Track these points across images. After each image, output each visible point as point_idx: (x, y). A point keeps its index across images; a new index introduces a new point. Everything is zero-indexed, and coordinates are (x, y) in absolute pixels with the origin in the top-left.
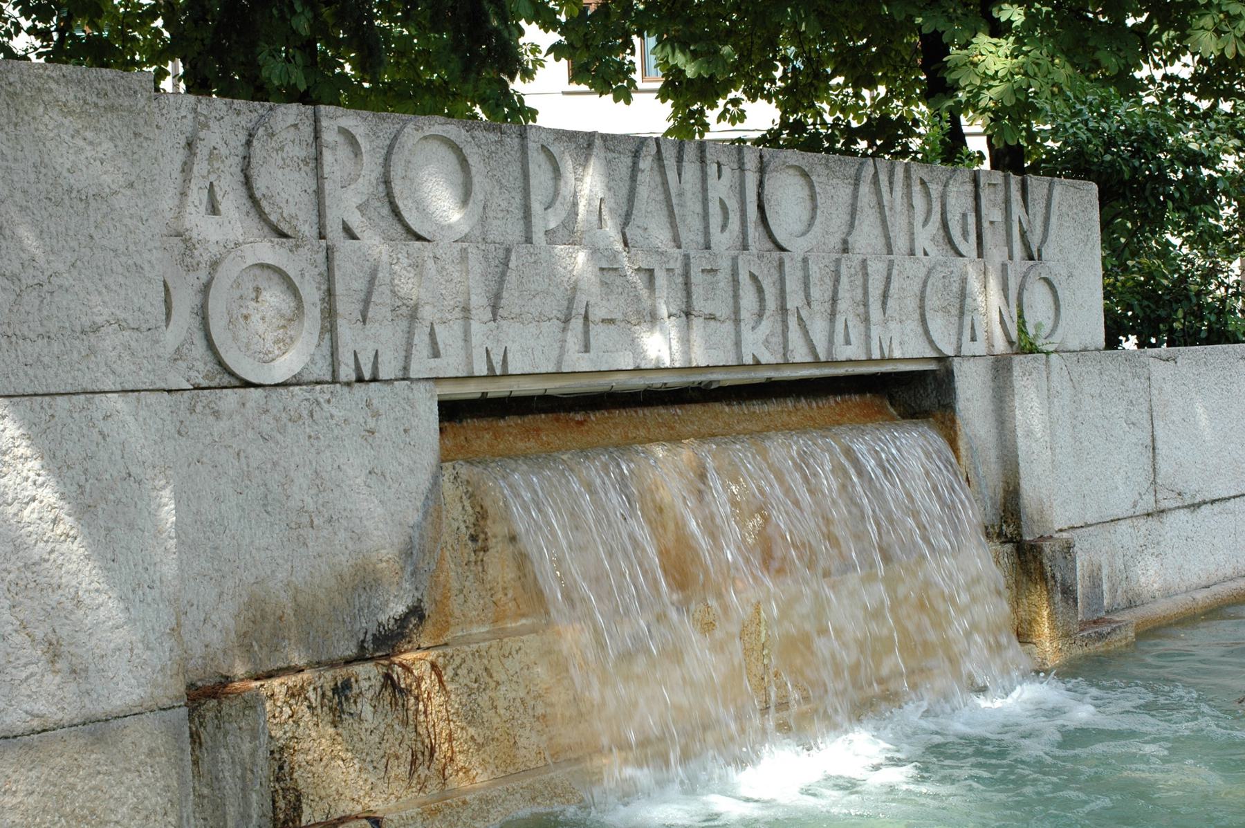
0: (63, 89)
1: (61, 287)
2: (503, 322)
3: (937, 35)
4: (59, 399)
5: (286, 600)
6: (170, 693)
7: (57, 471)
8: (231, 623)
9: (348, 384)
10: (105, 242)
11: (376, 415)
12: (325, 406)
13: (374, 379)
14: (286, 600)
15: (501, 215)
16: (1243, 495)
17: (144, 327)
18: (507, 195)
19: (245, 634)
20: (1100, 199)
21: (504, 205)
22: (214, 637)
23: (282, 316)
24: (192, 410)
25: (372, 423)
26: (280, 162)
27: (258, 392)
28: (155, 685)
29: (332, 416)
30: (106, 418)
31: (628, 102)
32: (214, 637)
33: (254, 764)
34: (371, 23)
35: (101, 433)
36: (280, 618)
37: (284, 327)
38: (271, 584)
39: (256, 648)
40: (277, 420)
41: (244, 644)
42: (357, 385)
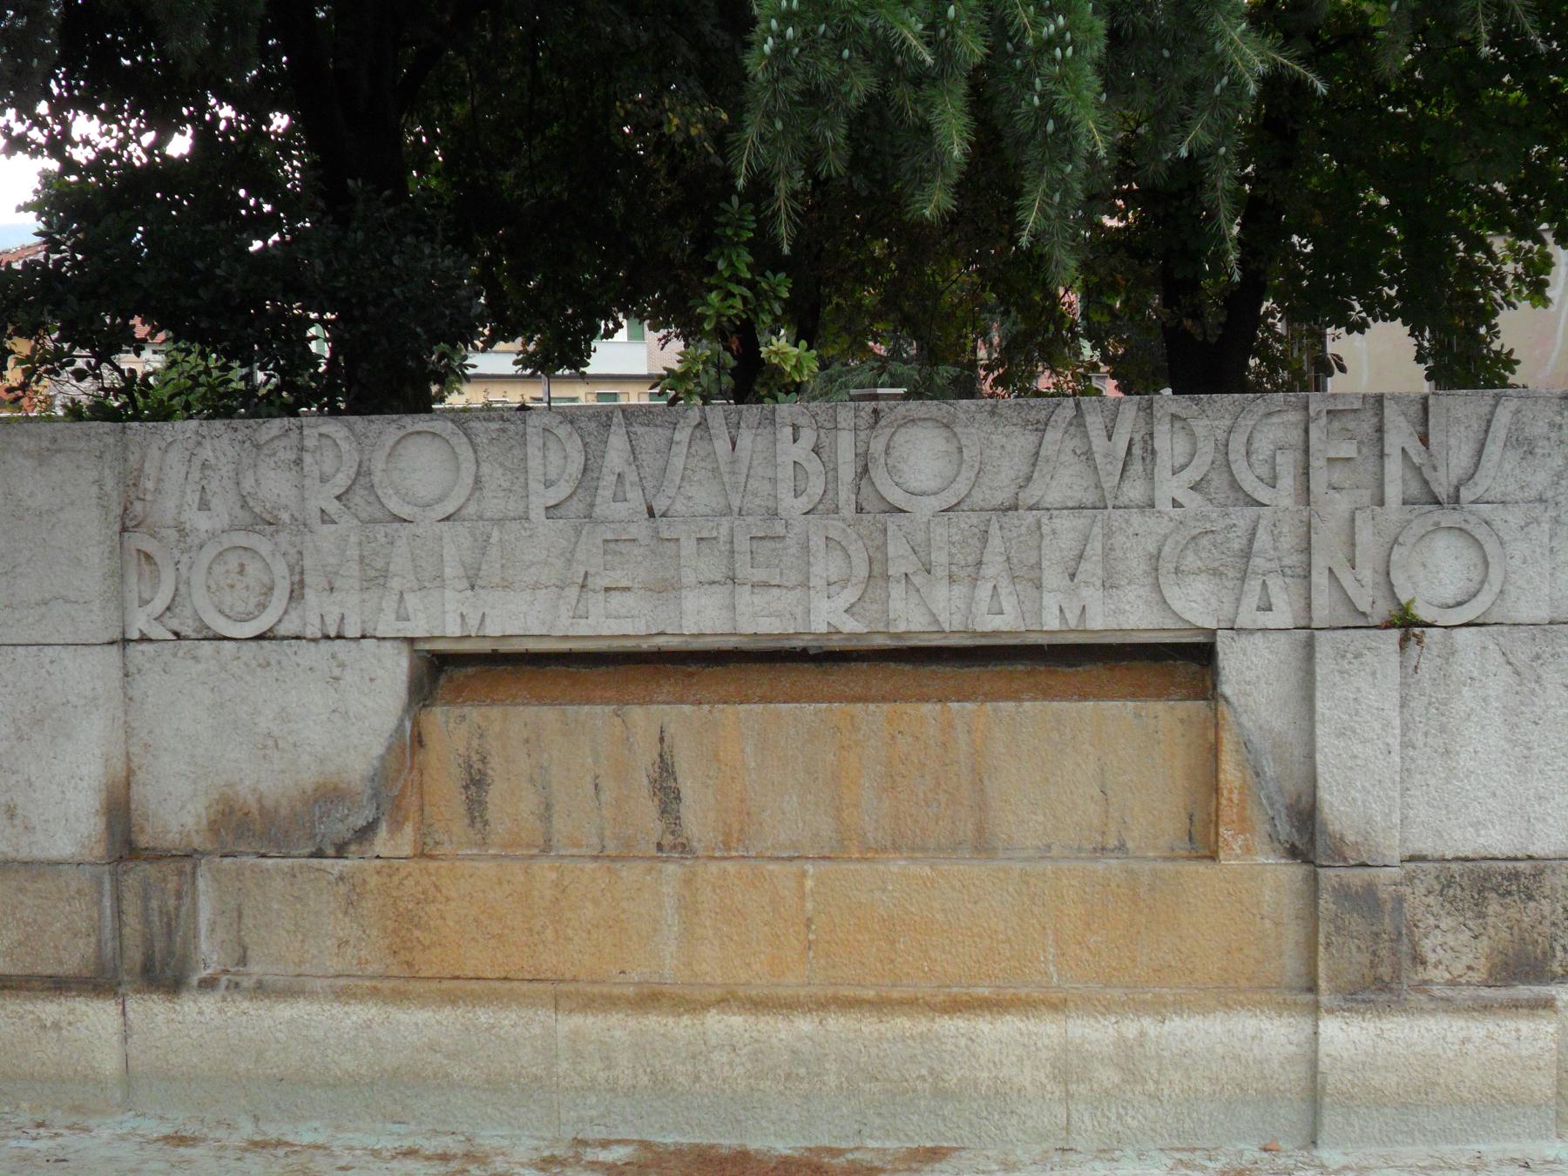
0: (26, 440)
1: (21, 574)
2: (481, 591)
3: (97, 224)
4: (19, 648)
5: (241, 801)
6: (95, 852)
7: (1370, 679)
8: (203, 813)
9: (314, 640)
10: (53, 543)
11: (342, 665)
12: (293, 657)
13: (339, 637)
14: (251, 801)
15: (501, 494)
16: (1566, 859)
17: (82, 600)
18: (509, 476)
19: (215, 821)
20: (1244, 392)
21: (506, 485)
22: (190, 822)
23: (265, 585)
24: (175, 655)
25: (337, 672)
26: (273, 465)
27: (232, 643)
28: (83, 846)
29: (298, 665)
30: (52, 662)
31: (1517, 362)
32: (190, 822)
33: (177, 916)
34: (92, 351)
35: (48, 672)
36: (246, 814)
37: (265, 594)
38: (239, 788)
39: (223, 833)
40: (247, 665)
41: (214, 827)
42: (322, 641)
